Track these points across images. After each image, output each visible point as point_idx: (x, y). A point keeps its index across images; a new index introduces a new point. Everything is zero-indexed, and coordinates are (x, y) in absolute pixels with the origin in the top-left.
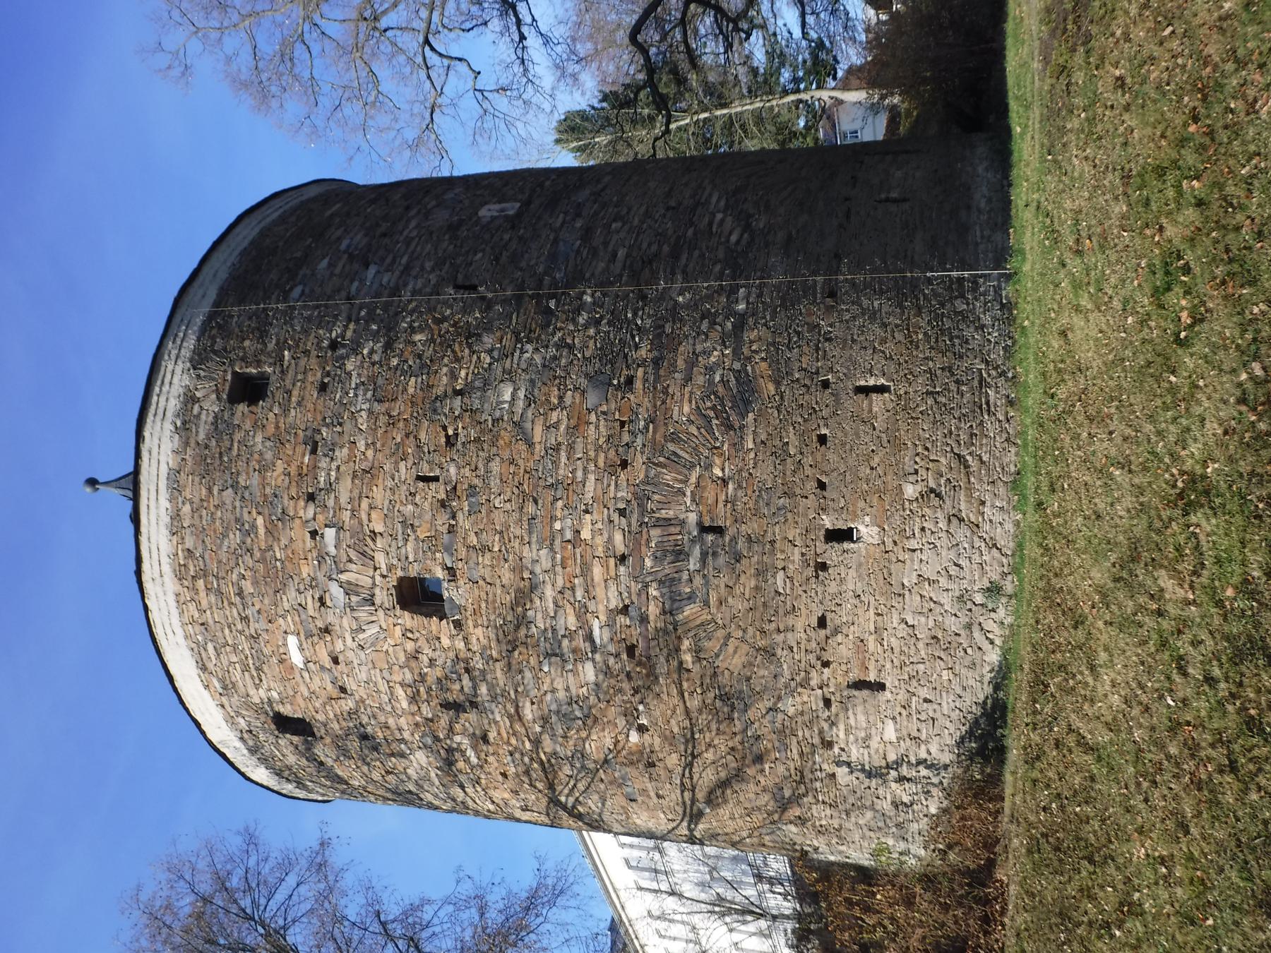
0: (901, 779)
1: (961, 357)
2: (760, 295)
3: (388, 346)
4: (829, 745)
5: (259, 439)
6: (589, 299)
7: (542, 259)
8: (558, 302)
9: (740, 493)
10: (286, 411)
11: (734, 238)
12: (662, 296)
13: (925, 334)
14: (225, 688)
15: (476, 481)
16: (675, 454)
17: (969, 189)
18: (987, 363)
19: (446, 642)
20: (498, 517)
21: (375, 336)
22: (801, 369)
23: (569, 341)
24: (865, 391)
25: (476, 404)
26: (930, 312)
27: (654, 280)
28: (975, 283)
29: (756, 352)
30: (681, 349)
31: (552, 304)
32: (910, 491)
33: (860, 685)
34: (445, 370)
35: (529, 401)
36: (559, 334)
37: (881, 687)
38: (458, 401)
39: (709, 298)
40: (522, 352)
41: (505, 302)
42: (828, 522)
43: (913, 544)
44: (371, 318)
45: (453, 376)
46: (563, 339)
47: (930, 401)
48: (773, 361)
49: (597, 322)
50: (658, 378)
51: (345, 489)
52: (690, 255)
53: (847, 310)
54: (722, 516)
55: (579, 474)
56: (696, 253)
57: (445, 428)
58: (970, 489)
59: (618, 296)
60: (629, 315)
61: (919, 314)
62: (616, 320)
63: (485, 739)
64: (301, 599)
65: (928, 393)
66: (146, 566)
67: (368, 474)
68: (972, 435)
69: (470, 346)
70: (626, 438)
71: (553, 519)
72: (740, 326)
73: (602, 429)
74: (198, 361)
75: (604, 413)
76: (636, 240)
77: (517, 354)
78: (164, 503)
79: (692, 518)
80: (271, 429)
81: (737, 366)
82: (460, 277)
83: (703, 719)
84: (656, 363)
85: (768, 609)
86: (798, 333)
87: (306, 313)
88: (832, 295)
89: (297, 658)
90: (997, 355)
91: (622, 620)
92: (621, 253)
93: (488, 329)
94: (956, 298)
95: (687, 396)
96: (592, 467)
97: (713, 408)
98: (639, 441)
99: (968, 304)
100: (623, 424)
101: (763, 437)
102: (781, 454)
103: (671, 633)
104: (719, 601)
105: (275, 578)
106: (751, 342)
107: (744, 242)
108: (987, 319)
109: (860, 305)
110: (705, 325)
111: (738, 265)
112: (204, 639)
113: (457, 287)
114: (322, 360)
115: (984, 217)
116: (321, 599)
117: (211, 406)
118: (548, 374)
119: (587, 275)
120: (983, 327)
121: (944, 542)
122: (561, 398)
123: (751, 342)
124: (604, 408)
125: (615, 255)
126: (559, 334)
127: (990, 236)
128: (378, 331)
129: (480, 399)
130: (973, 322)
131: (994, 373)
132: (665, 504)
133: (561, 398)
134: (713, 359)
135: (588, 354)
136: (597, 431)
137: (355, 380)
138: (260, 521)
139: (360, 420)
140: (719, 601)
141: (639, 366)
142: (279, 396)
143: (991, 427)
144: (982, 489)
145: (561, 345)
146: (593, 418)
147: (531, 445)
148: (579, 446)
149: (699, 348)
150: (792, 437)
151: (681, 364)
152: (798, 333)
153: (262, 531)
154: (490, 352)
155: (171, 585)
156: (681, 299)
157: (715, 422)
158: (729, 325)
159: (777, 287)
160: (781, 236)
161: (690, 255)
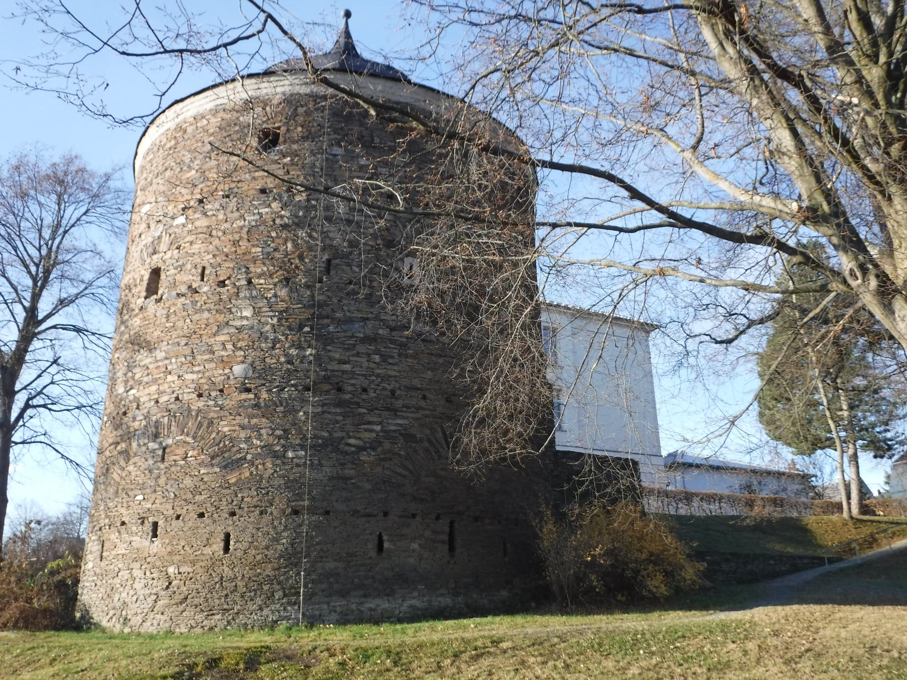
1: (242, 597)
2: (298, 465)
3: (285, 227)
6: (308, 353)
7: (348, 314)
8: (308, 332)
9: (179, 468)
11: (352, 441)
13: (260, 574)
15: (199, 304)
16: (202, 426)
17: (388, 595)
18: (237, 613)
22: (243, 498)
23: (278, 346)
25: (242, 295)
26: (275, 576)
28: (295, 604)
29: (257, 467)
30: (264, 420)
31: (307, 329)
34: (265, 269)
35: (240, 329)
36: (283, 338)
38: (244, 282)
40: (271, 317)
43: (148, 573)
46: (279, 341)
47: (217, 579)
49: (289, 362)
50: (246, 408)
52: (340, 414)
53: (280, 523)
54: (170, 458)
55: (196, 369)
56: (341, 418)
57: (229, 278)
59: (308, 371)
60: (292, 382)
61: (274, 570)
65: (222, 577)
66: (181, 105)
68: (196, 606)
69: (280, 281)
70: (213, 394)
71: (177, 357)
73: (220, 378)
74: (291, 101)
75: (229, 378)
76: (358, 375)
77: (271, 314)
79: (170, 441)
81: (249, 457)
82: (338, 261)
84: (257, 406)
86: (267, 493)
87: (317, 164)
88: (296, 512)
90: (241, 619)
92: (347, 367)
94: (284, 592)
95: (233, 428)
96: (200, 376)
97: (225, 446)
98: (211, 403)
99: (279, 599)
100: (221, 391)
101: (205, 479)
102: (196, 491)
106: (264, 464)
107: (347, 448)
108: (266, 612)
109: (284, 531)
110: (278, 432)
111: (325, 447)
113: (329, 261)
115: (354, 607)
118: (256, 336)
119: (329, 348)
120: (261, 609)
121: (147, 592)
122: (240, 348)
123: (264, 464)
124: (232, 377)
125: (345, 363)
126: (283, 338)
127: (335, 611)
128: (297, 217)
129: (245, 297)
130: (265, 603)
131: (230, 618)
133: (240, 348)
134: (255, 441)
135: (267, 360)
136: (218, 374)
137: (263, 211)
139: (238, 222)
141: (256, 395)
145: (275, 341)
146: (227, 371)
148: (213, 365)
149: (263, 431)
151: (254, 421)
152: (267, 493)
154: (275, 296)
156: (301, 413)
157: (216, 448)
158: (278, 448)
159: (303, 476)
160: (349, 472)
161: (340, 414)
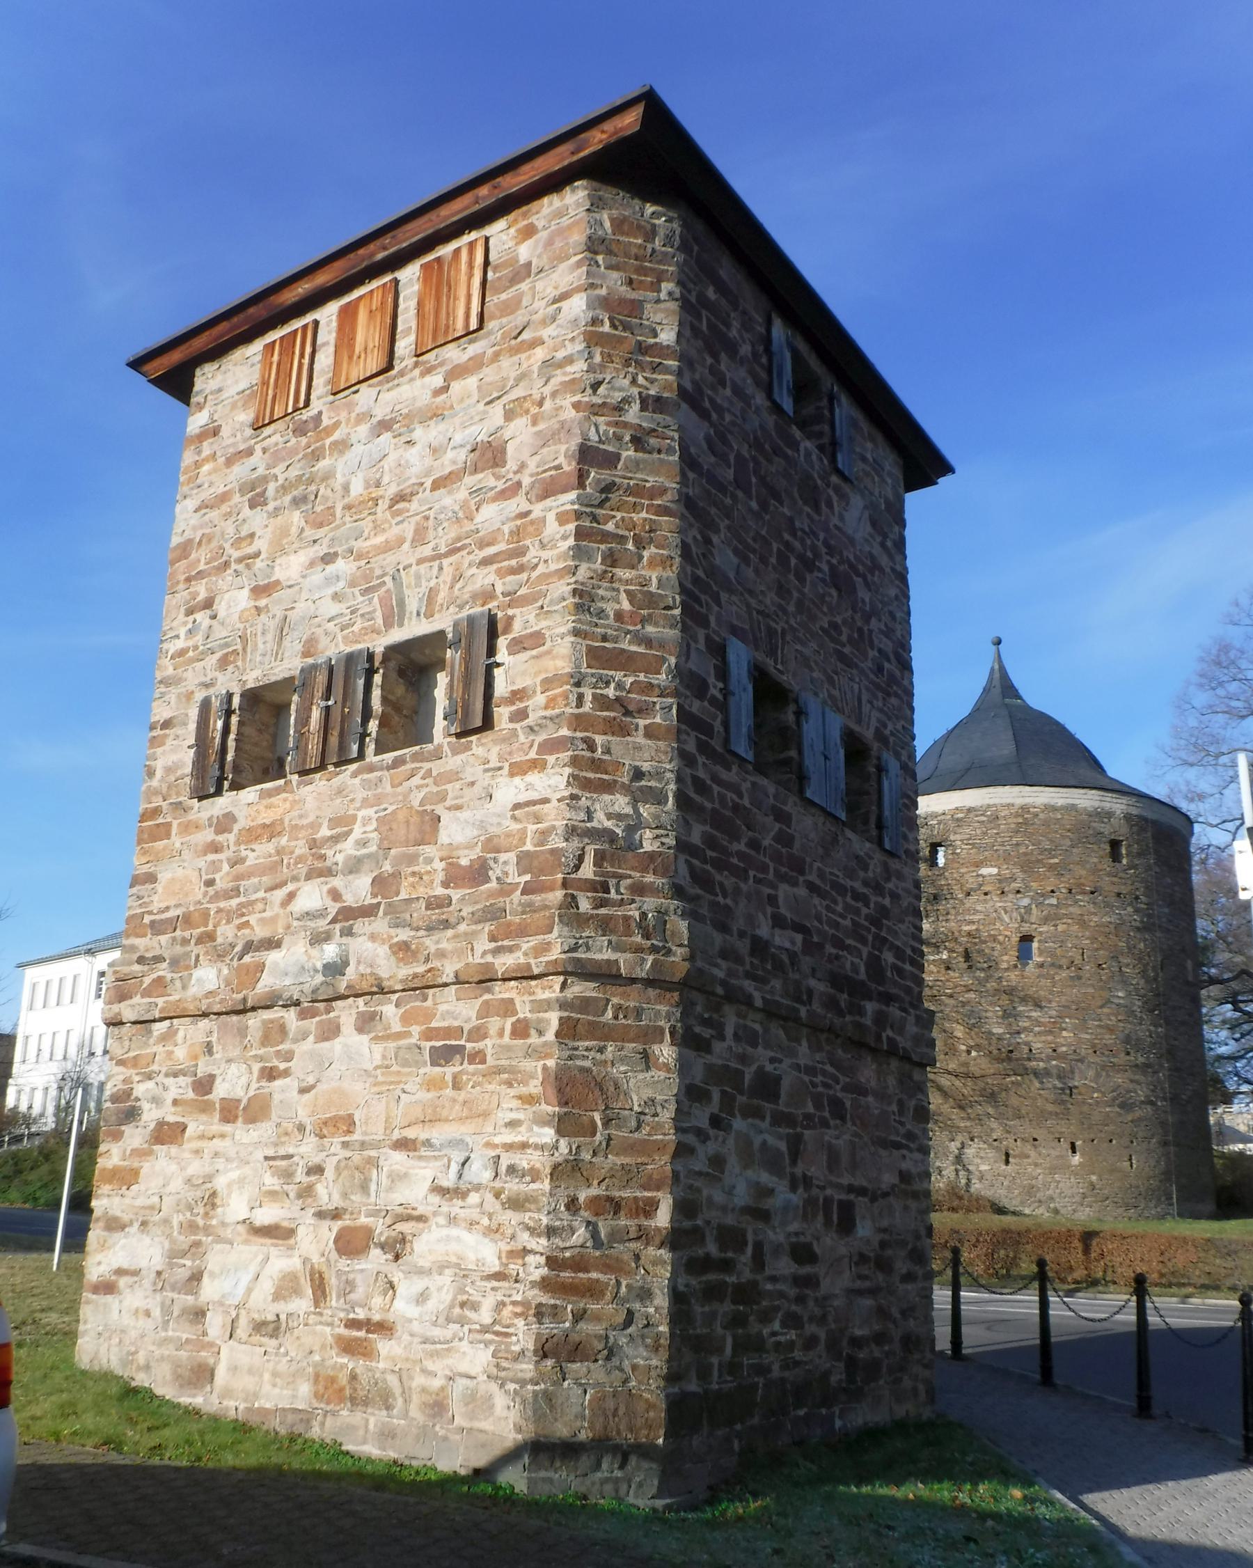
0: (957, 1171)
3: (1138, 929)
4: (972, 1140)
5: (1095, 860)
10: (1109, 875)
12: (1161, 1066)
14: (958, 820)
19: (1005, 958)
20: (1067, 991)
21: (1142, 922)
24: (1130, 1160)
27: (1168, 1061)
32: (1094, 1178)
33: (1007, 1155)
37: (1007, 1162)
39: (1162, 1089)
41: (1157, 988)
42: (1078, 1143)
44: (1149, 916)
45: (1127, 965)
48: (1140, 1119)
51: (1075, 910)
58: (1095, 1202)
62: (1153, 1045)
63: (948, 968)
64: (1019, 880)
67: (1083, 923)
72: (1152, 1103)
74: (1128, 817)
78: (1060, 802)
80: (1100, 867)
83: (981, 1084)
85: (1043, 1116)
89: (985, 871)
91: (1026, 1050)
93: (1147, 982)
103: (1025, 1072)
104: (1039, 1093)
105: (1028, 865)
112: (993, 817)
114: (1130, 893)
116: (1018, 892)
117: (1106, 829)
132: (1081, 1071)
136: (1109, 1039)
138: (1056, 861)
140: (1039, 1093)
142: (1114, 870)
143: (1120, 1210)
144: (1096, 1207)
147: (1101, 1007)
150: (1112, 1127)
153: (1052, 861)
155: (1019, 802)
